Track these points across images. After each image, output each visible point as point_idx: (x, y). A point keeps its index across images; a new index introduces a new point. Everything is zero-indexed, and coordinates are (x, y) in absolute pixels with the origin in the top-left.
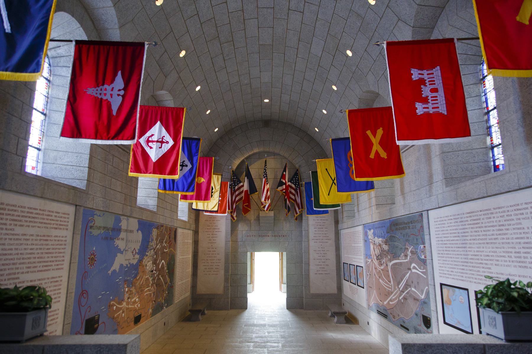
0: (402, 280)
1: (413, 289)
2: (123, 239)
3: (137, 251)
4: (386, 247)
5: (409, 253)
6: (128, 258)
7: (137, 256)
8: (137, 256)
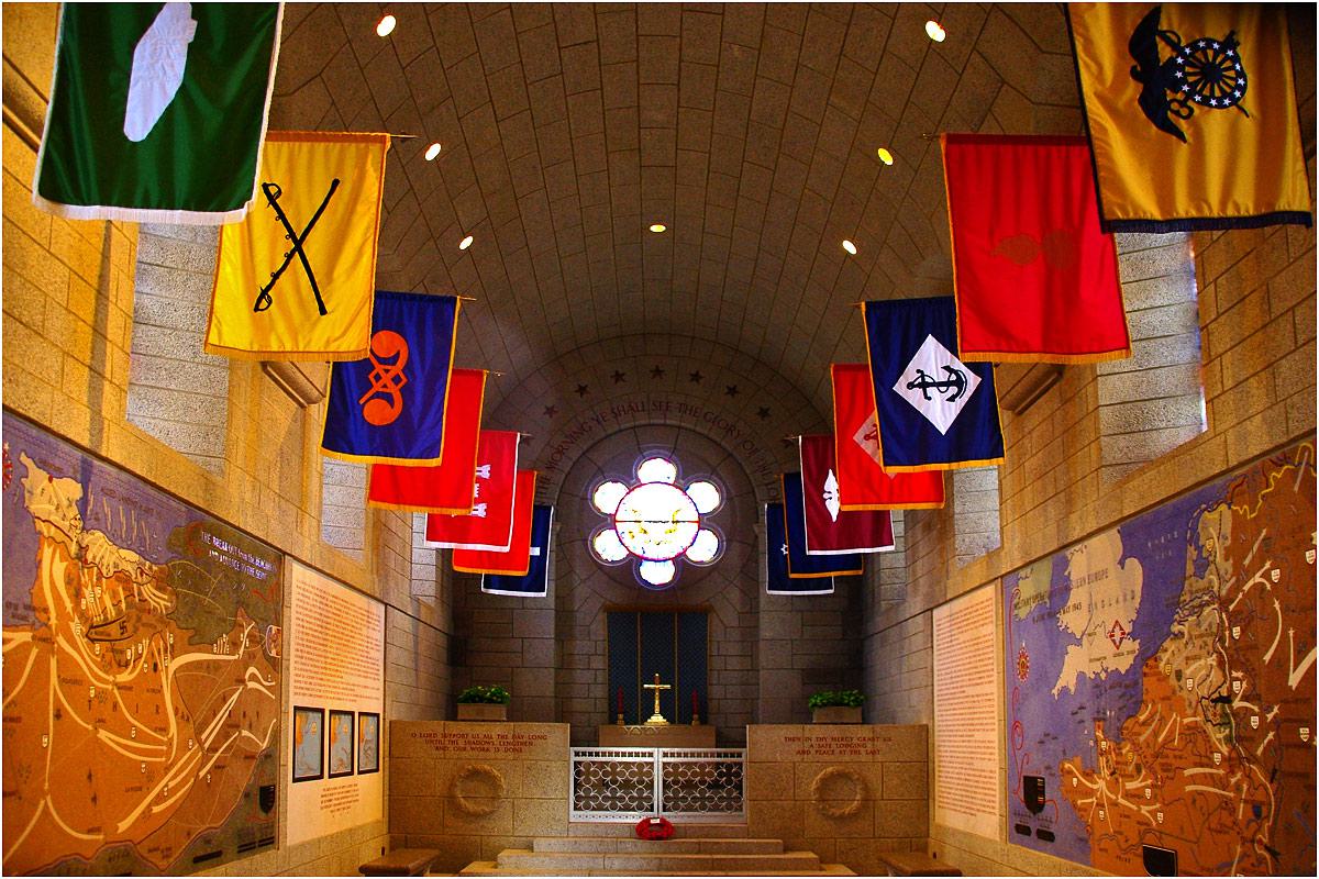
0: (215, 715)
1: (245, 733)
2: (1077, 607)
3: (1128, 628)
4: (160, 601)
5: (244, 638)
6: (1098, 656)
7: (1132, 645)
8: (1132, 645)
